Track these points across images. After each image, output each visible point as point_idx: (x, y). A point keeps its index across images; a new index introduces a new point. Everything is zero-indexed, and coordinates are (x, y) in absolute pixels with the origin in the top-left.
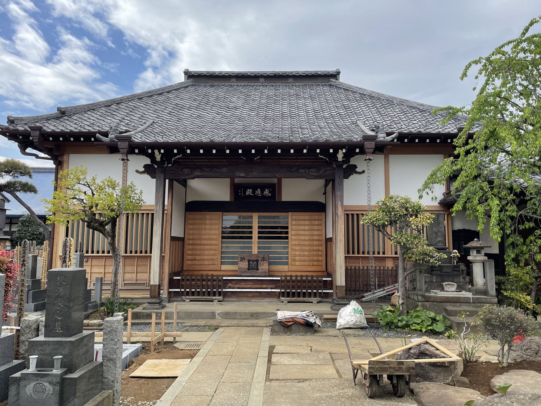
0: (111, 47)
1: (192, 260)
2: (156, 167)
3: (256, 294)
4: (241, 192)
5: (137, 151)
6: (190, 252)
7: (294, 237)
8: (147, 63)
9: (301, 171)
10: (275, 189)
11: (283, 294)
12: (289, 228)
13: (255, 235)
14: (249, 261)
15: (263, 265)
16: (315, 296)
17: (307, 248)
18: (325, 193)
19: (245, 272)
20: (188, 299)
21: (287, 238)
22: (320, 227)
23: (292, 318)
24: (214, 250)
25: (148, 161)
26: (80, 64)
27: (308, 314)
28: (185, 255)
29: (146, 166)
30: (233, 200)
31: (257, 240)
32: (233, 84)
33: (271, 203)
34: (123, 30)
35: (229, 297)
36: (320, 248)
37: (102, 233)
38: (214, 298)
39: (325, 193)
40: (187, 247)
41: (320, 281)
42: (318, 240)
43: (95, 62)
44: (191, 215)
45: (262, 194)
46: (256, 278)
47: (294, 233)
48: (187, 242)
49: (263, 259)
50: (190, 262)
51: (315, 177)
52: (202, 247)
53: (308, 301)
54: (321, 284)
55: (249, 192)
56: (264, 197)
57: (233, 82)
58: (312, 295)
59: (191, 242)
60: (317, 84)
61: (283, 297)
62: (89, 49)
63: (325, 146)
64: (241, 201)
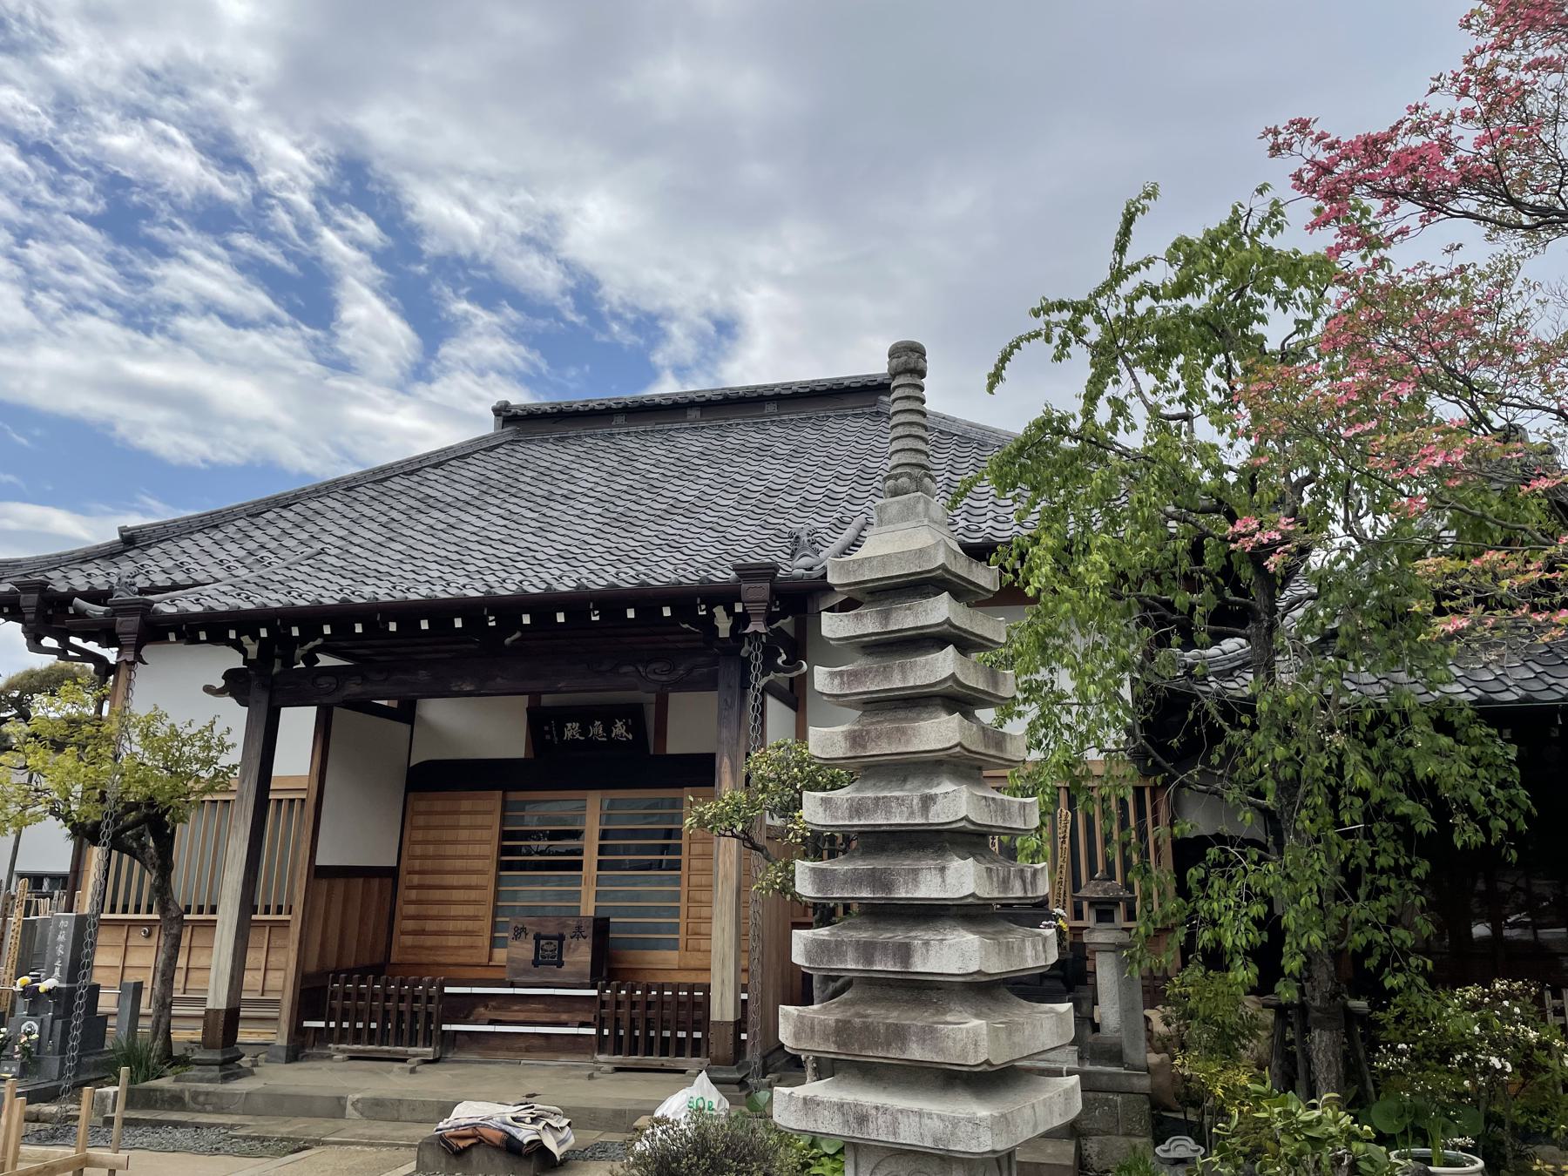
0: (573, 325)
1: (415, 933)
3: (536, 1042)
4: (550, 732)
5: (203, 636)
8: (658, 358)
9: (624, 669)
11: (601, 1044)
13: (590, 858)
14: (538, 938)
19: (526, 972)
20: (344, 1051)
21: (675, 865)
23: (474, 1126)
24: (475, 902)
26: (493, 376)
27: (520, 1115)
32: (616, 430)
34: (600, 274)
35: (461, 1048)
38: (412, 1050)
40: (403, 894)
43: (534, 366)
45: (609, 736)
48: (404, 879)
50: (408, 940)
53: (672, 1066)
55: (572, 730)
56: (613, 743)
59: (416, 879)
60: (841, 412)
62: (517, 335)
64: (555, 761)
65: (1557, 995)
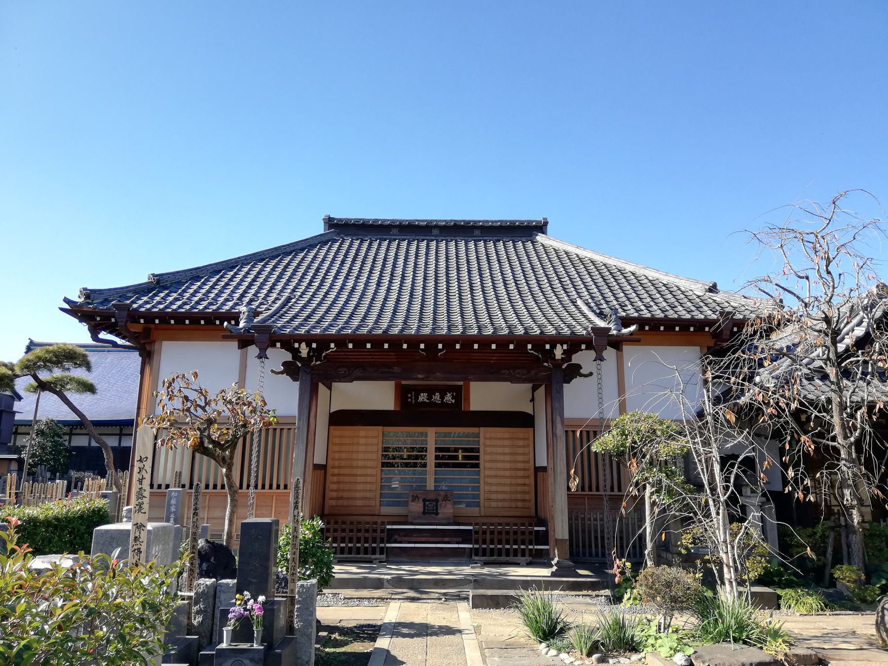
1: (337, 498)
2: (300, 365)
4: (411, 398)
6: (335, 487)
7: (488, 465)
9: (504, 371)
10: (461, 394)
11: (476, 552)
12: (481, 450)
13: (431, 460)
14: (424, 500)
15: (445, 506)
16: (523, 555)
17: (508, 481)
18: (532, 400)
19: (419, 518)
21: (477, 466)
22: (526, 450)
25: (288, 357)
28: (327, 491)
29: (285, 364)
30: (398, 409)
31: (433, 468)
33: (457, 415)
35: (396, 555)
36: (527, 481)
37: (215, 459)
38: (373, 557)
39: (532, 400)
40: (330, 478)
41: (531, 533)
42: (525, 469)
44: (338, 431)
46: (439, 527)
47: (488, 457)
48: (330, 471)
49: (446, 498)
50: (334, 503)
51: (523, 381)
52: (352, 479)
54: (533, 537)
55: (423, 397)
56: (444, 405)
57: (394, 235)
58: (519, 554)
59: (336, 471)
61: (477, 555)
63: (540, 341)
64: (408, 413)
65: (885, 521)
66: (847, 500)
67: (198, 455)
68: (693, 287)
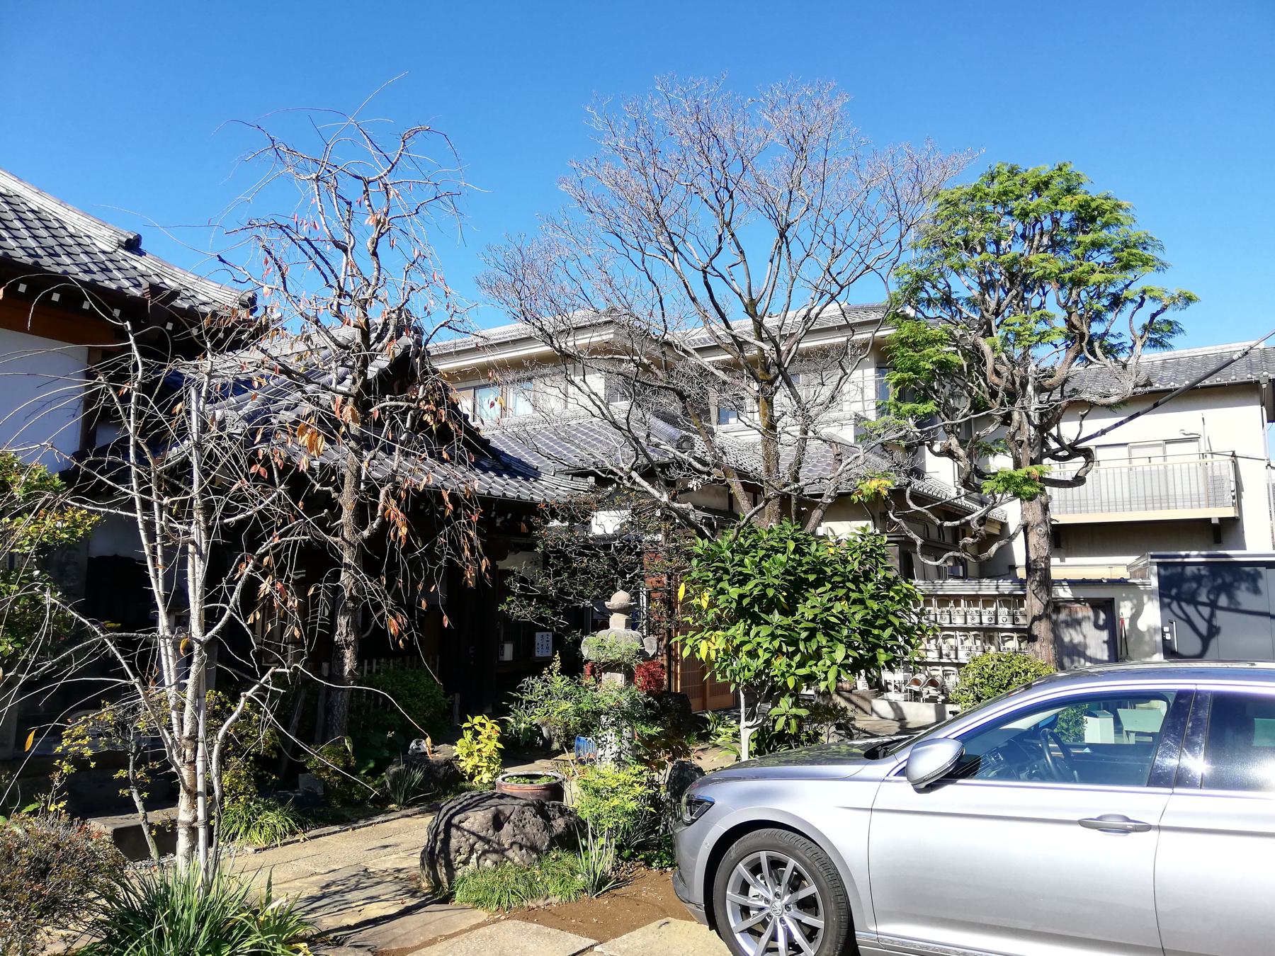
66: (341, 634)
67: (1162, 707)
68: (93, 232)
